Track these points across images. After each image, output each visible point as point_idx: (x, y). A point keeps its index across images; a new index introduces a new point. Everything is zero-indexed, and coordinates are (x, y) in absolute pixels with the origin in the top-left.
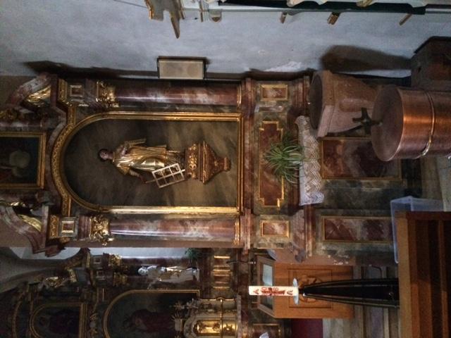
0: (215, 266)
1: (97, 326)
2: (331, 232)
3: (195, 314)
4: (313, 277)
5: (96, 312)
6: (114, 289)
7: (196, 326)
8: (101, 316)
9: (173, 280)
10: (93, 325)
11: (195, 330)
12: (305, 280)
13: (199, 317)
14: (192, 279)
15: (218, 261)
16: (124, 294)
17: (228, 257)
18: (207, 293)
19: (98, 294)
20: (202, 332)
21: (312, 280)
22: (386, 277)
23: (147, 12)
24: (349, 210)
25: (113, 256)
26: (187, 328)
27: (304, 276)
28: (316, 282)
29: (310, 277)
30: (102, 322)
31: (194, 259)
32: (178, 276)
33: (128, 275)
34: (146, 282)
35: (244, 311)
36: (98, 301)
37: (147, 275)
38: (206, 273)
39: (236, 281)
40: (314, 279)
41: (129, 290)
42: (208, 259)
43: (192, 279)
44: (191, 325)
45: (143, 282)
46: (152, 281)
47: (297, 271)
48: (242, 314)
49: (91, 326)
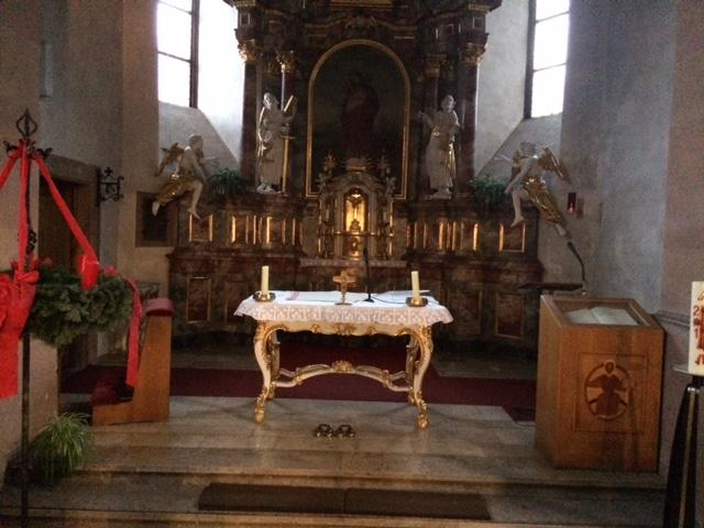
0: (463, 226)
1: (357, 28)
2: (111, 465)
3: (376, 192)
4: (631, 399)
5: (380, 26)
6: (416, 57)
7: (360, 192)
8: (370, 34)
9: (432, 152)
10: (361, 21)
11: (353, 191)
12: (626, 385)
13: (373, 198)
14: (432, 186)
15: (469, 230)
16: (404, 72)
17: (475, 248)
18: (407, 211)
19: (406, 28)
20: (348, 202)
21: (625, 397)
22: (29, 515)
23: (142, 190)
24: (104, 470)
25: (484, 51)
26: (361, 178)
27: (633, 384)
28: (621, 406)
29: (631, 395)
30: (361, 37)
31: (471, 190)
32: (442, 163)
33: (440, 78)
34: (426, 109)
35: (384, 271)
36: (395, 28)
37: (440, 109)
38: (450, 210)
39: (430, 261)
40: (626, 400)
41: (411, 81)
42: (474, 214)
43: (432, 186)
44: (362, 183)
45: (427, 100)
46: (433, 118)
47: (645, 371)
48: (382, 268)
49: (358, 18)
